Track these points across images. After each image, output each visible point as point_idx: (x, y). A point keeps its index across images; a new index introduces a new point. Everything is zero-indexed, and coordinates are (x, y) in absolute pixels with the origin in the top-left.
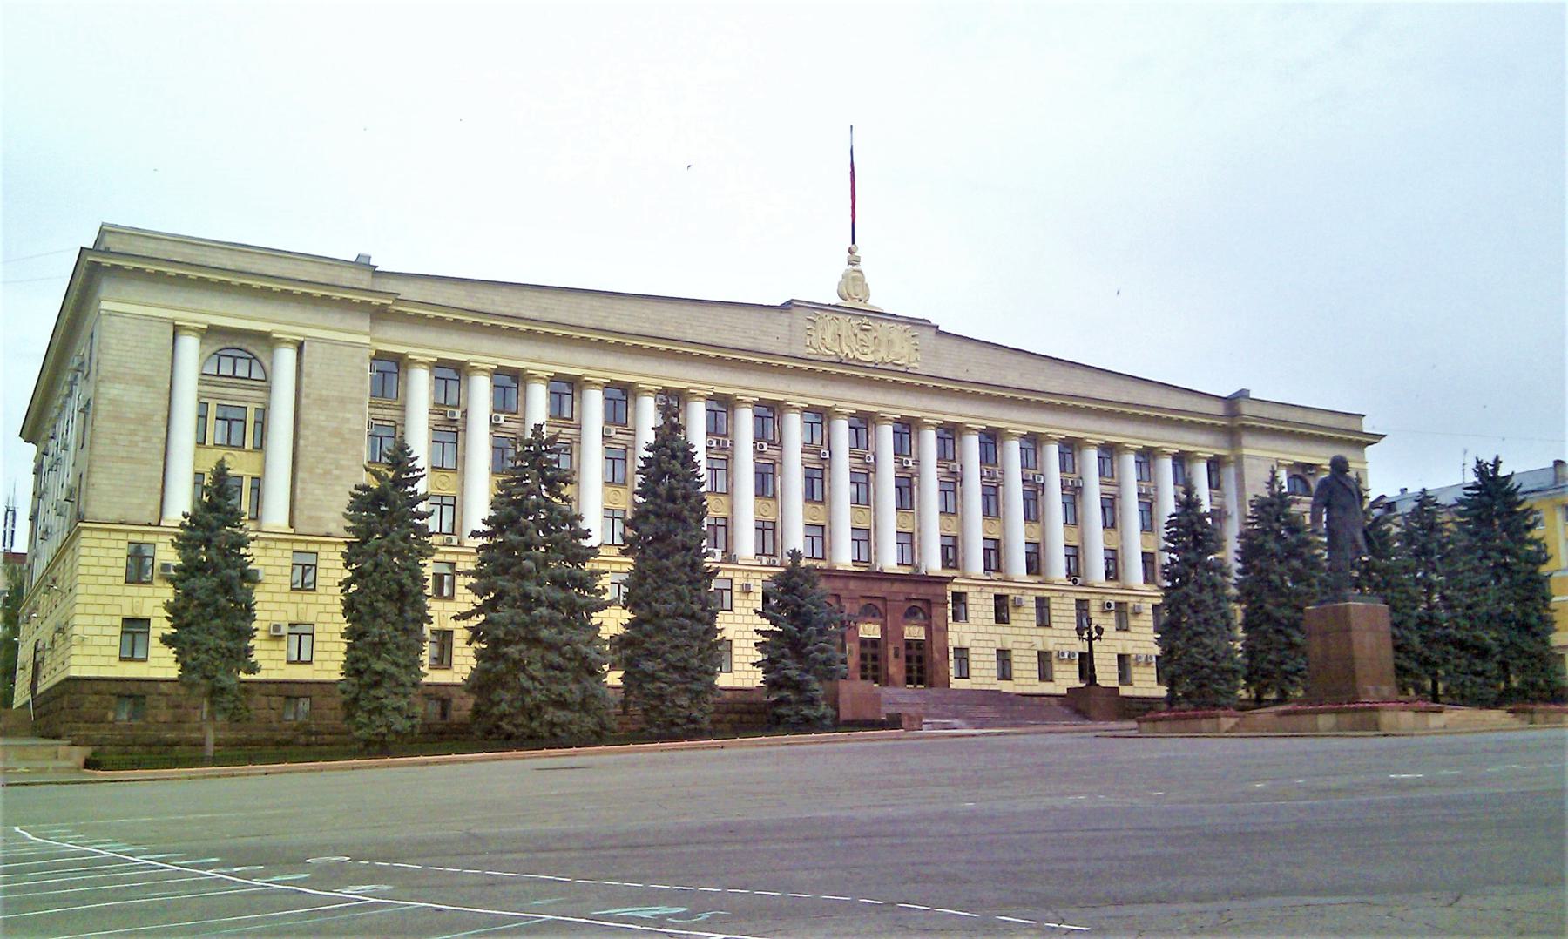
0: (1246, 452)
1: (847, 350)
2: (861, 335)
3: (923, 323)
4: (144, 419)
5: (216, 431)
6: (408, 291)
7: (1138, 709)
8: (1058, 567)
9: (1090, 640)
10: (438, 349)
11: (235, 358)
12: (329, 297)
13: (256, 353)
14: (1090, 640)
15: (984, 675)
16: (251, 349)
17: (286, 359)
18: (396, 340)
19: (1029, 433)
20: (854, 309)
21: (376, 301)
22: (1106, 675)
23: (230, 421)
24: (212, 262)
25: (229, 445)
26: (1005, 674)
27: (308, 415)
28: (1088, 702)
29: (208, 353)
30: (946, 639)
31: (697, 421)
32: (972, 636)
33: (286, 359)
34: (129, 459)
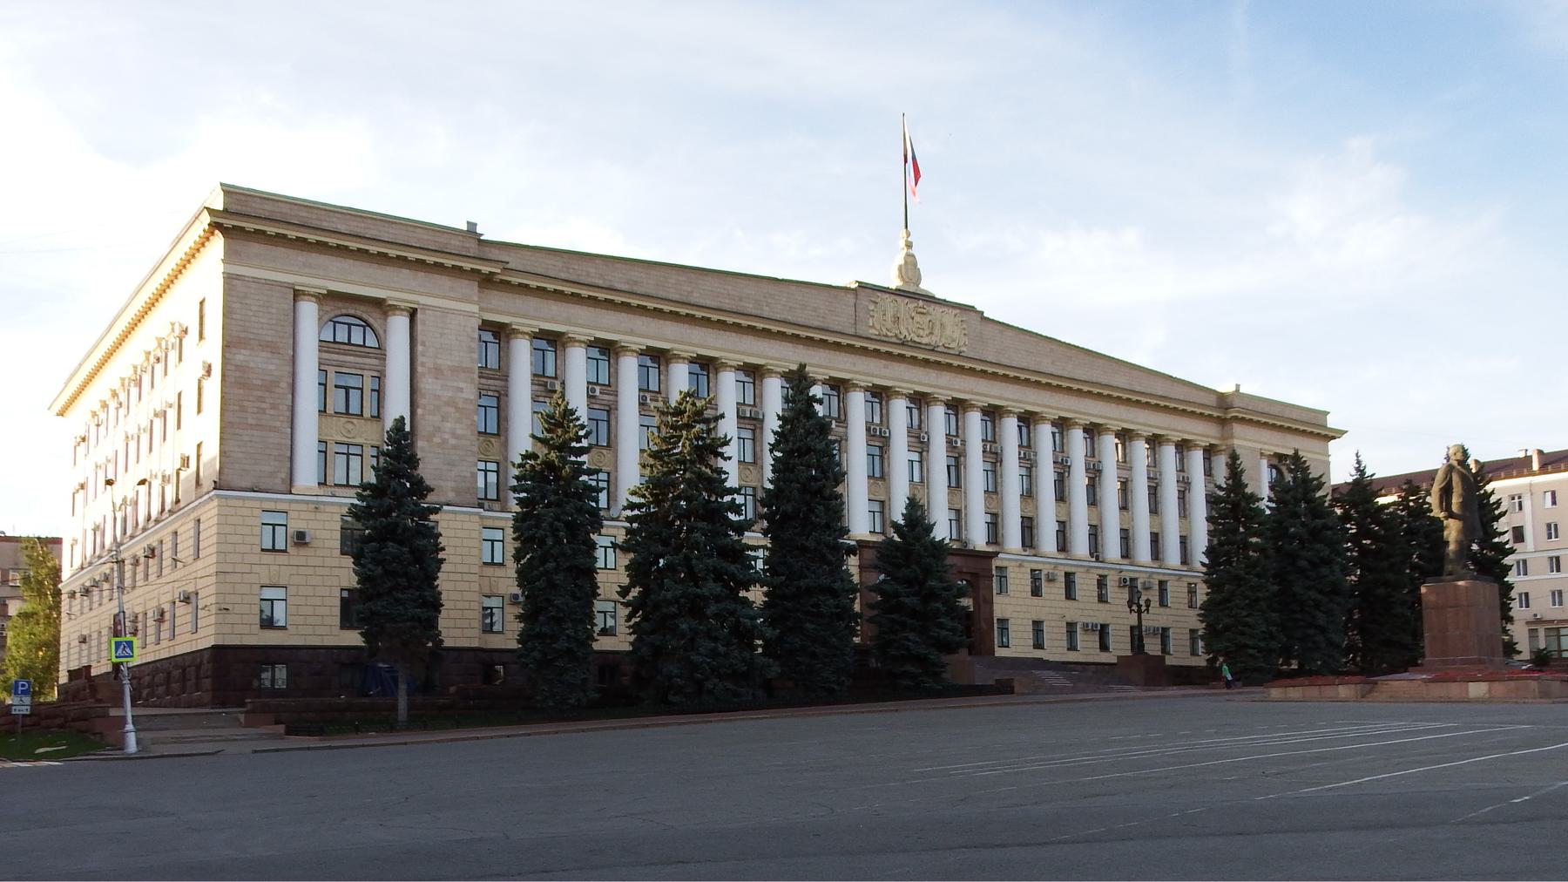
0: (1236, 442)
1: (905, 332)
2: (918, 318)
3: (971, 309)
4: (269, 387)
5: (336, 400)
6: (514, 261)
7: (1184, 677)
8: (1081, 545)
9: (1139, 612)
10: (742, 353)
11: (349, 325)
12: (284, 236)
13: (371, 321)
14: (1139, 612)
15: (1019, 645)
16: (365, 316)
17: (398, 326)
18: (503, 308)
19: (1027, 412)
20: (912, 295)
21: (486, 269)
22: (1152, 647)
23: (347, 389)
24: (342, 228)
25: (347, 413)
26: (1104, 647)
27: (427, 384)
28: (1146, 669)
29: (326, 318)
30: (992, 611)
31: (578, 368)
32: (294, 570)
33: (398, 326)
34: (258, 427)
